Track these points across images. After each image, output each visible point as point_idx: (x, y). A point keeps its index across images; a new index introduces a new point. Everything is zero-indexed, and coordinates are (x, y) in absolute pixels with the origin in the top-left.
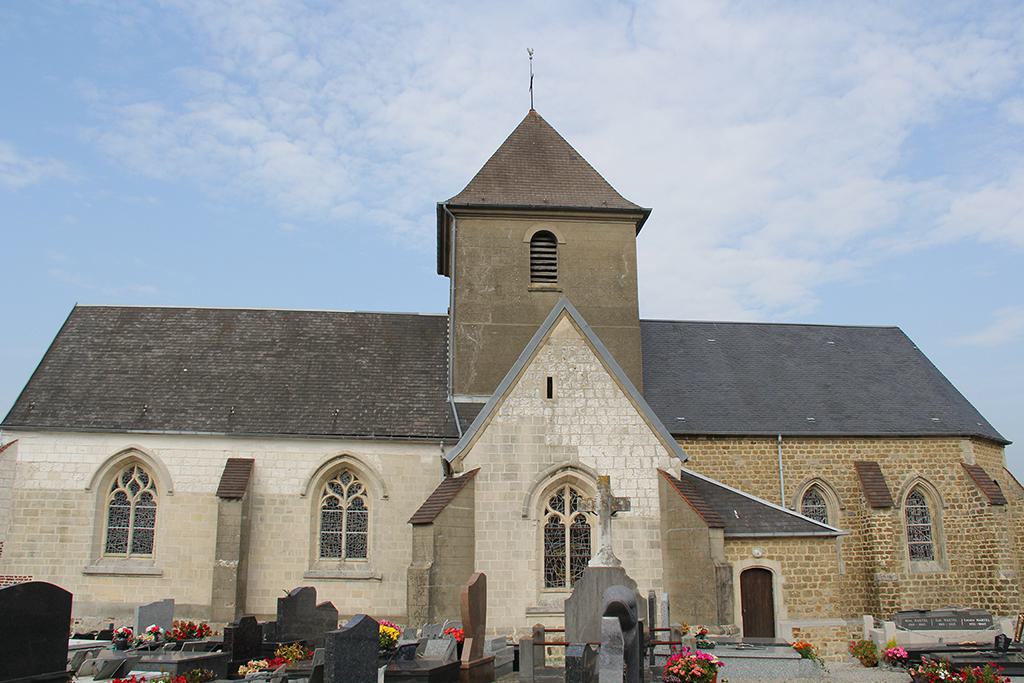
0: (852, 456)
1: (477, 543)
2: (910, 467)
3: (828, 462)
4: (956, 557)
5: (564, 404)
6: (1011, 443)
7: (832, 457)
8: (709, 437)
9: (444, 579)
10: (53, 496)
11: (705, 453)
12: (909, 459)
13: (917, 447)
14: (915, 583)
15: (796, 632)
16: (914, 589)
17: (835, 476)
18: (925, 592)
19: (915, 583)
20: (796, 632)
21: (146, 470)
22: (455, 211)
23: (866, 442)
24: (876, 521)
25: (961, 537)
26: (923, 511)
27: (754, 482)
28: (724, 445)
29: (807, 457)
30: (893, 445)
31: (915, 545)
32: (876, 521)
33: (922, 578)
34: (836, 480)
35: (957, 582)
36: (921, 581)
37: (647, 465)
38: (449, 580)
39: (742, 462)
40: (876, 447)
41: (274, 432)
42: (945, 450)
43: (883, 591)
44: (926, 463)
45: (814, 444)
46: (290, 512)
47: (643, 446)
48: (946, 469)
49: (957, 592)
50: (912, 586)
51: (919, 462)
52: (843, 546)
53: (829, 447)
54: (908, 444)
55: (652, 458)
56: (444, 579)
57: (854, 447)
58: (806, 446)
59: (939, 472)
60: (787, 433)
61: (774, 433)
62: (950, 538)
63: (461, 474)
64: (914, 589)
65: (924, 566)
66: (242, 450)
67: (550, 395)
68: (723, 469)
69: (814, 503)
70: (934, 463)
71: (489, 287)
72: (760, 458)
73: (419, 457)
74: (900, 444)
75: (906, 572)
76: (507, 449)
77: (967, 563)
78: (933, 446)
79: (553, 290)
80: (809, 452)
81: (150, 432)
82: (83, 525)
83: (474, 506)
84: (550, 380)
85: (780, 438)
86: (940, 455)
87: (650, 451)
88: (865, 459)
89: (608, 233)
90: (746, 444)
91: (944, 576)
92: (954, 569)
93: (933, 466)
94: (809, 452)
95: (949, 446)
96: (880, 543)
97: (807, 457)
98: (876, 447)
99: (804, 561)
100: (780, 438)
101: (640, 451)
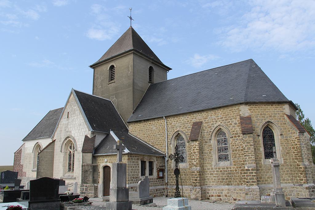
0: (193, 120)
2: (216, 121)
3: (184, 124)
4: (236, 159)
7: (185, 122)
8: (144, 120)
9: (42, 169)
11: (144, 126)
13: (220, 112)
14: (217, 171)
16: (216, 174)
18: (221, 175)
19: (217, 171)
22: (93, 67)
23: (198, 114)
24: (192, 146)
25: (239, 150)
26: (225, 139)
28: (150, 123)
29: (176, 123)
30: (210, 113)
32: (192, 146)
34: (186, 131)
35: (236, 170)
36: (219, 170)
37: (84, 134)
38: (44, 169)
39: (154, 128)
40: (203, 115)
42: (233, 112)
44: (224, 119)
45: (179, 118)
48: (233, 120)
49: (236, 175)
50: (215, 173)
51: (221, 118)
53: (184, 118)
54: (209, 113)
55: (85, 132)
56: (42, 169)
57: (194, 116)
58: (176, 119)
59: (229, 122)
60: (166, 115)
61: (161, 116)
62: (233, 151)
64: (216, 174)
65: (223, 164)
69: (181, 141)
70: (227, 118)
72: (160, 126)
74: (212, 112)
75: (213, 166)
78: (227, 110)
79: (113, 83)
80: (177, 121)
81: (40, 138)
83: (54, 150)
85: (164, 117)
86: (230, 114)
87: (85, 129)
88: (198, 121)
90: (156, 121)
91: (230, 168)
92: (235, 165)
94: (177, 121)
95: (235, 109)
96: (194, 155)
97: (176, 123)
98: (203, 115)
100: (164, 117)
101: (83, 130)
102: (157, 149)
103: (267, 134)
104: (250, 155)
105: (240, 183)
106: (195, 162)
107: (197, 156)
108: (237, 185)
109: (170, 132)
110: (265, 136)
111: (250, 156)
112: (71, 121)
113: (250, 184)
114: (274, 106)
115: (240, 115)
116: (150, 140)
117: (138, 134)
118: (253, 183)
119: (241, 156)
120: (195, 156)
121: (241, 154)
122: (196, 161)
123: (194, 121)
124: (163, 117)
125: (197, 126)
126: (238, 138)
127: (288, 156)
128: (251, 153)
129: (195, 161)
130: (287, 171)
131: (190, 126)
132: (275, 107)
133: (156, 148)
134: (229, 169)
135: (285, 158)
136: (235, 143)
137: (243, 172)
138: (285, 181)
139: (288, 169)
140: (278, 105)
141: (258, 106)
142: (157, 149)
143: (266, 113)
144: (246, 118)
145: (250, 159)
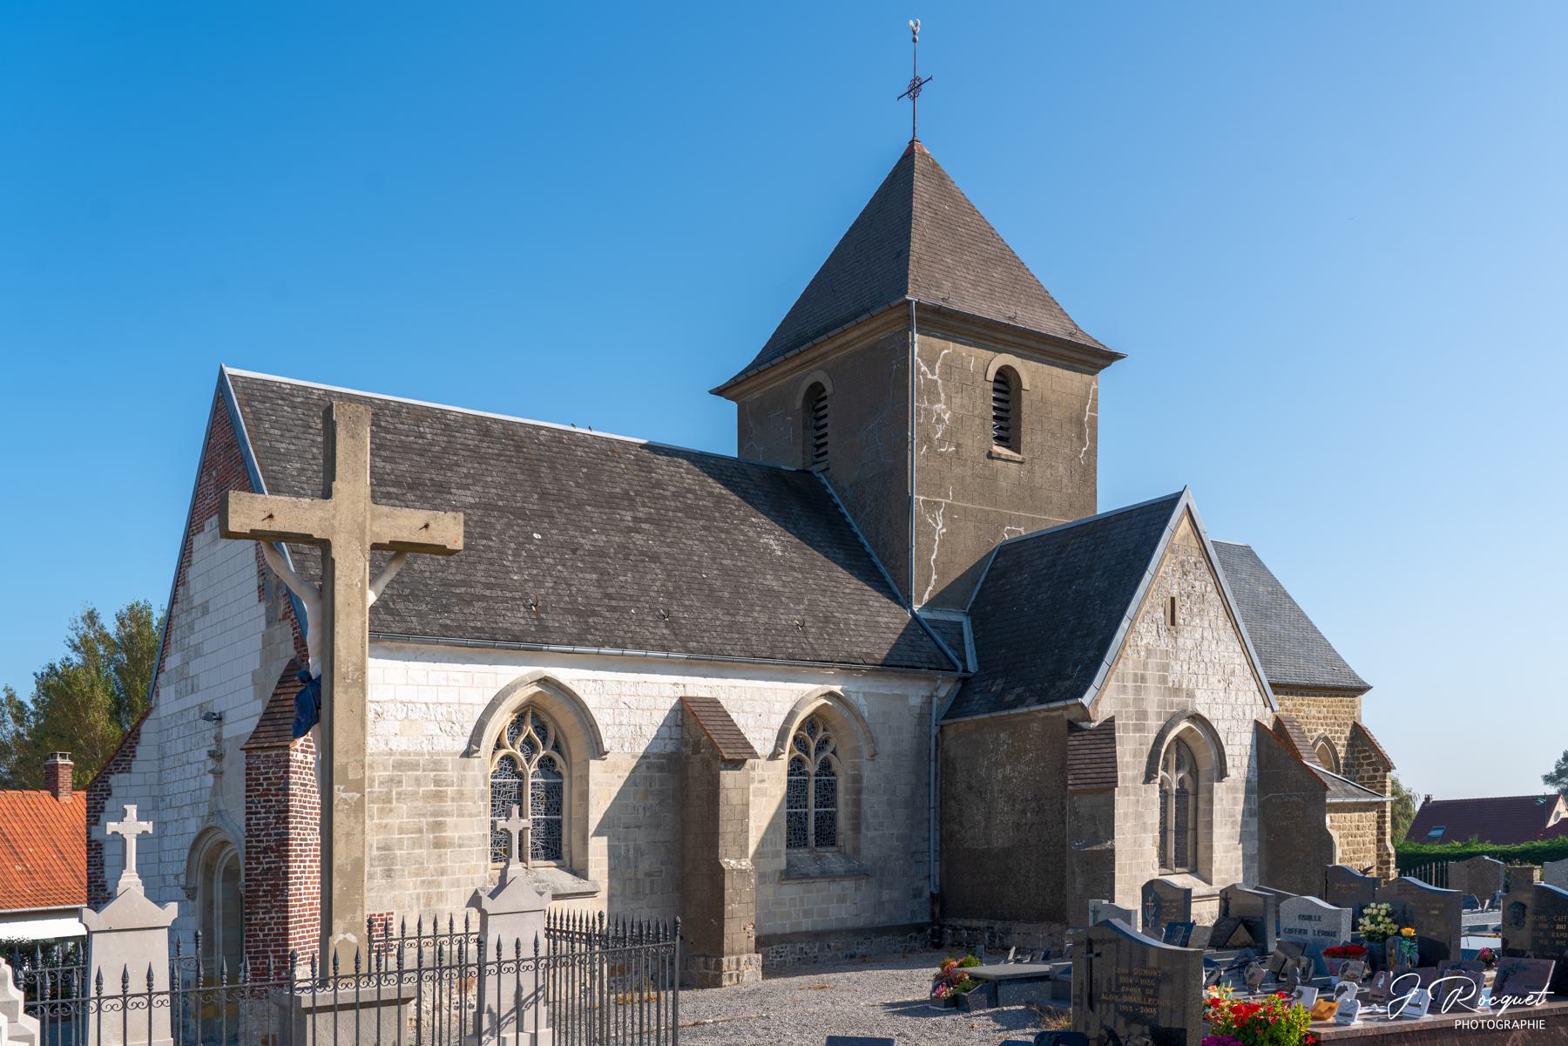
10: (414, 766)
21: (544, 718)
41: (408, 635)
46: (763, 781)
63: (1097, 724)
66: (699, 686)
67: (1173, 623)
71: (950, 446)
73: (907, 697)
76: (1138, 690)
82: (471, 815)
84: (1173, 599)
89: (1065, 380)
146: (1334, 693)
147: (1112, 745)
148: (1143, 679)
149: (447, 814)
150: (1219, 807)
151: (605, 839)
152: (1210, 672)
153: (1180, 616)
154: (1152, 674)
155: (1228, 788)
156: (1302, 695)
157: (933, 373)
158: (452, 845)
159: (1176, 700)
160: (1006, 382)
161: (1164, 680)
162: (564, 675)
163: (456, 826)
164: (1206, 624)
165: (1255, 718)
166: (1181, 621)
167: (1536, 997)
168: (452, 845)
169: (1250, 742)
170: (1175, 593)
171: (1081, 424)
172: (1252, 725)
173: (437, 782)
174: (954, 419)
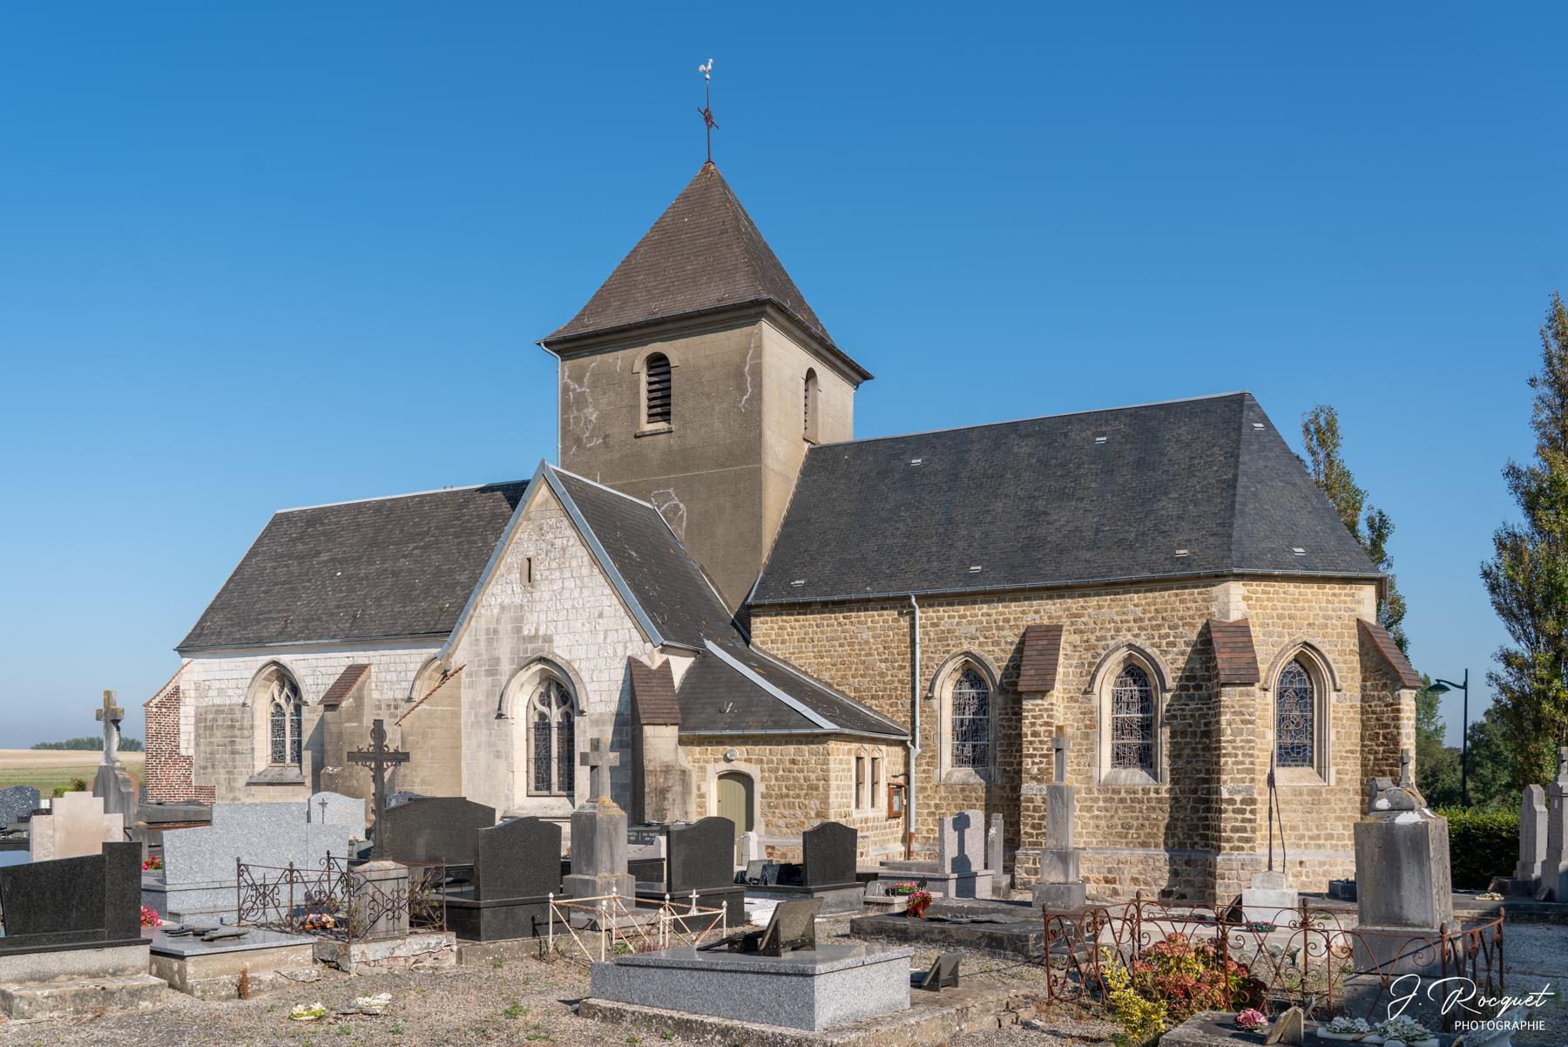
1: (463, 745)
2: (1118, 630)
5: (543, 592)
6: (108, 694)
10: (222, 712)
12: (1118, 618)
15: (769, 850)
17: (996, 649)
20: (769, 850)
25: (1194, 733)
27: (881, 661)
31: (1124, 745)
33: (1119, 793)
36: (1116, 797)
42: (1182, 601)
43: (1027, 809)
47: (617, 631)
52: (1001, 745)
59: (1168, 636)
68: (841, 645)
72: (890, 628)
76: (490, 641)
77: (1199, 772)
88: (1046, 622)
93: (1159, 627)
96: (1031, 743)
97: (958, 624)
99: (787, 765)
102: (875, 712)
103: (1291, 682)
104: (1240, 753)
105: (1188, 842)
106: (1036, 767)
107: (1045, 747)
108: (1177, 847)
109: (930, 655)
110: (1285, 691)
111: (1240, 758)
112: (546, 596)
113: (1231, 845)
114: (1327, 590)
115: (1209, 614)
116: (844, 677)
117: (793, 653)
118: (1241, 844)
119: (1198, 755)
120: (1037, 745)
121: (1200, 746)
122: (1041, 762)
123: (1031, 619)
124: (910, 598)
125: (1045, 642)
126: (1196, 693)
127: (1352, 761)
128: (1242, 747)
129: (1037, 764)
130: (1344, 810)
131: (1011, 637)
132: (1331, 592)
133: (870, 708)
134: (1152, 795)
135: (1341, 767)
136: (1183, 710)
137: (1203, 806)
138: (1334, 842)
139: (1346, 805)
140: (1339, 588)
141: (1274, 586)
142: (875, 712)
143: (1298, 613)
144: (1233, 629)
145: (1240, 767)
146: (1032, 595)
147: (1055, 652)
148: (496, 631)
149: (236, 737)
150: (582, 739)
151: (310, 752)
152: (571, 616)
153: (537, 575)
154: (506, 628)
155: (591, 721)
156: (1083, 596)
157: (581, 385)
158: (239, 753)
159: (530, 646)
160: (658, 363)
161: (519, 630)
162: (285, 659)
163: (240, 743)
164: (567, 575)
165: (629, 653)
166: (538, 577)
167: (1535, 998)
168: (239, 753)
169: (622, 677)
170: (530, 554)
171: (742, 375)
172: (625, 661)
173: (232, 720)
174: (600, 418)
